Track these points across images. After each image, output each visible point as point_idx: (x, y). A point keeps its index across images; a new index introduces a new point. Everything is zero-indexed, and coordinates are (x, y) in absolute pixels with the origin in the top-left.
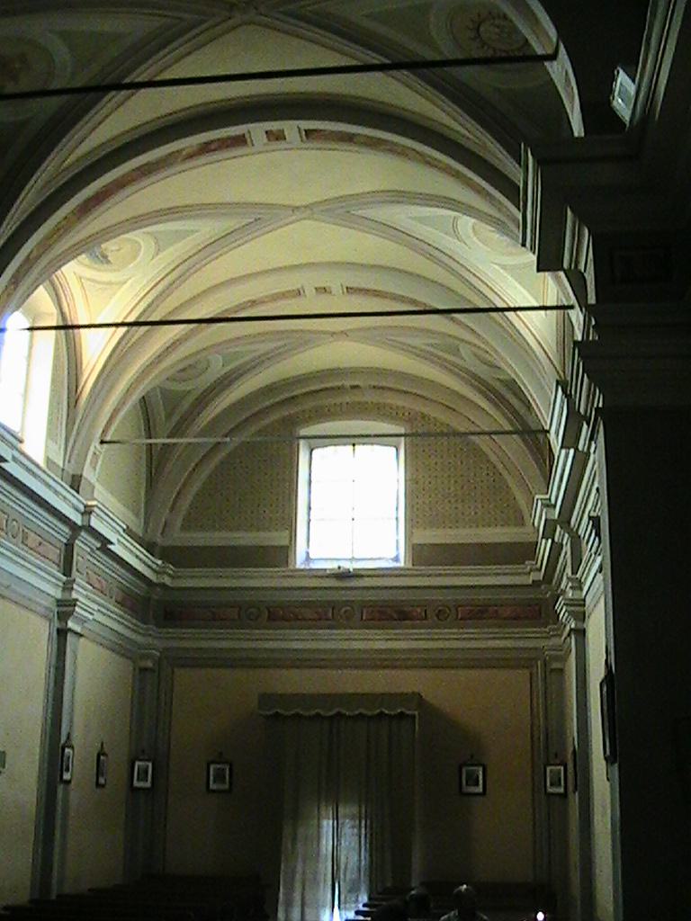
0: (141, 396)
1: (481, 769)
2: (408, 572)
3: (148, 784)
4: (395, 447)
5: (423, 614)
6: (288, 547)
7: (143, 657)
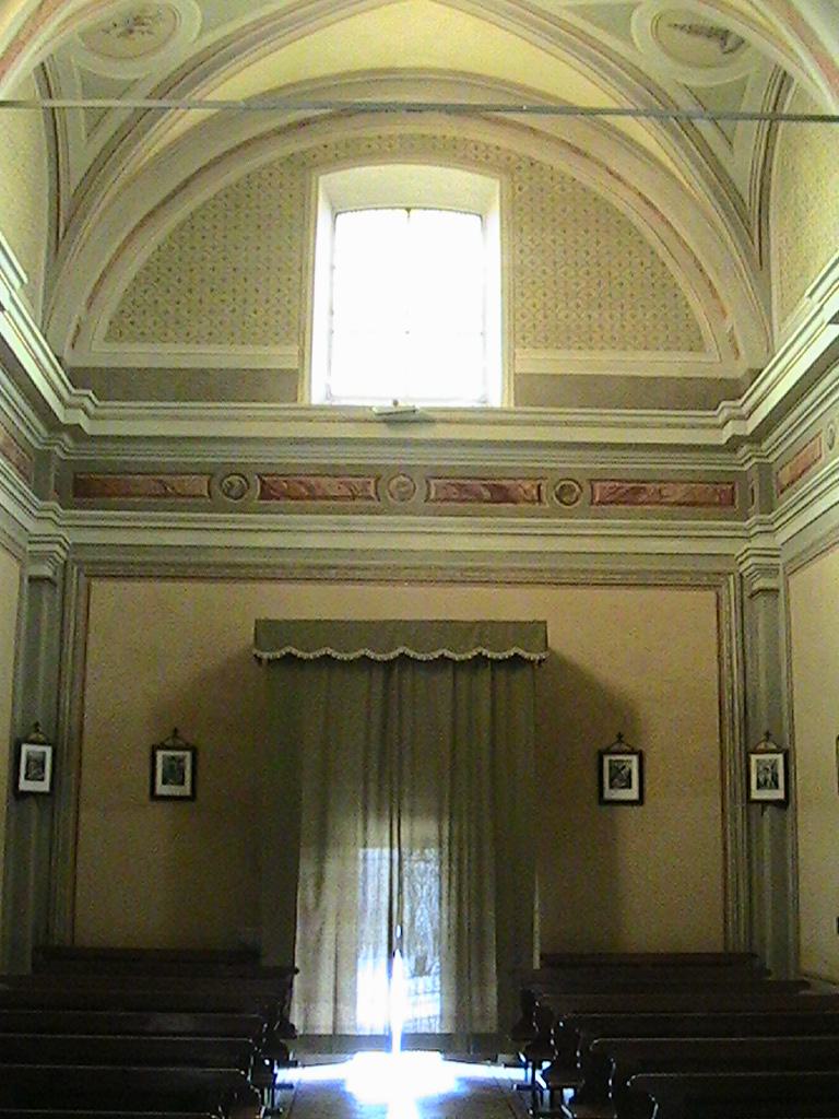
0: (37, 63)
1: (635, 759)
2: (509, 417)
3: (44, 786)
4: (481, 216)
5: (535, 492)
6: (295, 372)
7: (38, 558)
